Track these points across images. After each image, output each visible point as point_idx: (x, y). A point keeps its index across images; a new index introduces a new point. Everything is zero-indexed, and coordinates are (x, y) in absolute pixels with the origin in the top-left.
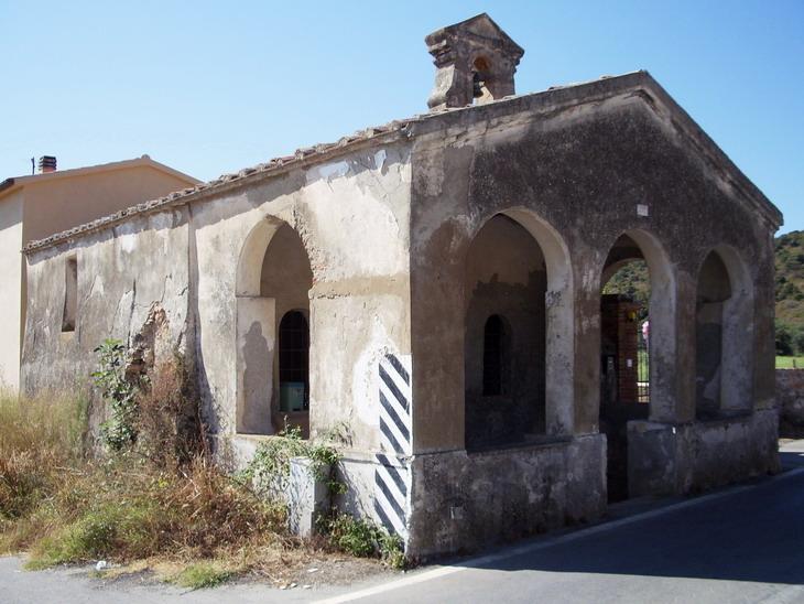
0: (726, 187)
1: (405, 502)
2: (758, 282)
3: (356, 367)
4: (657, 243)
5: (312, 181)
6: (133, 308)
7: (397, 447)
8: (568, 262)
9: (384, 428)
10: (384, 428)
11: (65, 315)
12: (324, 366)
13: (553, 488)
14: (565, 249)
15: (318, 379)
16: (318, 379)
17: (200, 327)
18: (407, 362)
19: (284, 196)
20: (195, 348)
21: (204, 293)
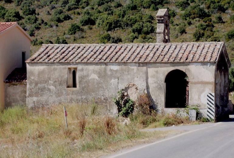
0: (226, 60)
1: (213, 114)
2: (76, 9)
3: (201, 95)
4: (229, 72)
5: (191, 65)
6: (118, 83)
7: (211, 106)
8: (219, 78)
9: (208, 104)
10: (208, 104)
11: (67, 83)
12: (193, 95)
13: (39, 85)
14: (219, 76)
15: (191, 97)
16: (191, 97)
17: (149, 88)
18: (213, 94)
19: (182, 66)
20: (148, 92)
21: (150, 80)
